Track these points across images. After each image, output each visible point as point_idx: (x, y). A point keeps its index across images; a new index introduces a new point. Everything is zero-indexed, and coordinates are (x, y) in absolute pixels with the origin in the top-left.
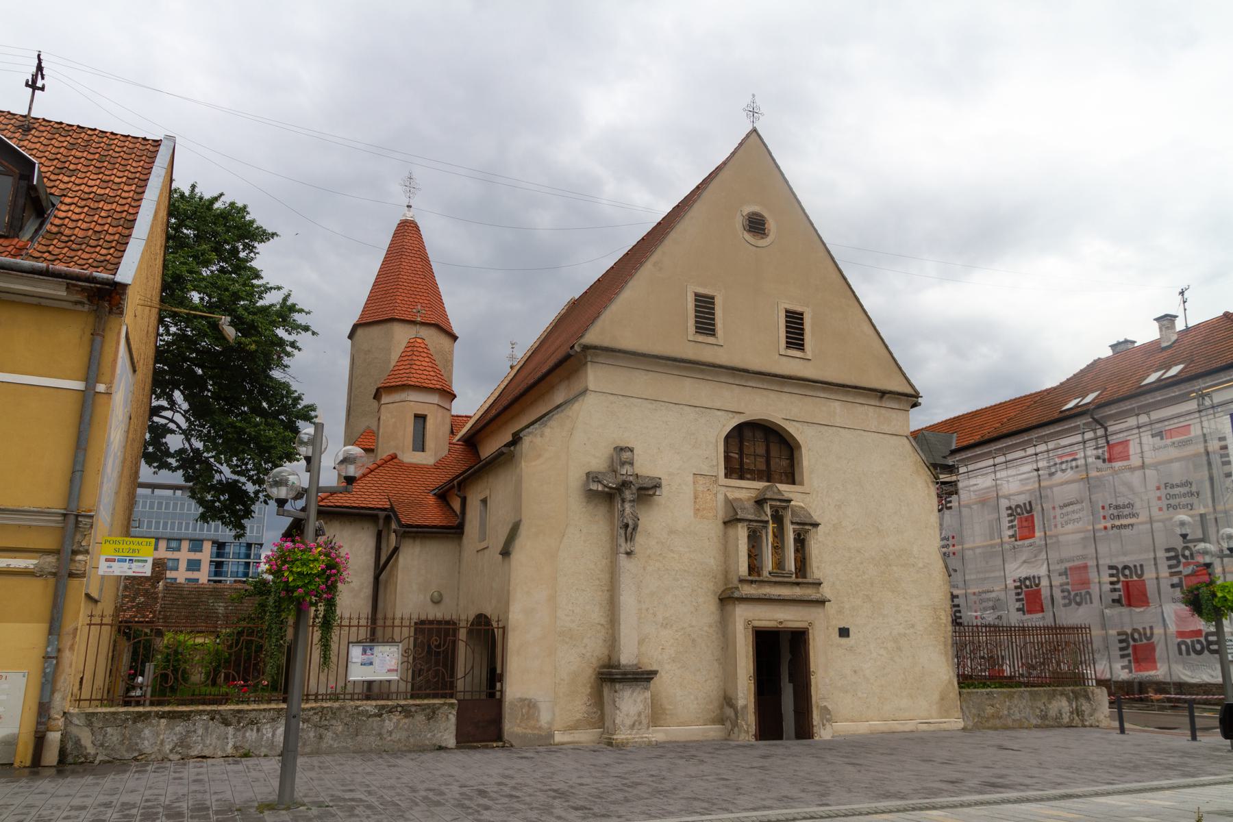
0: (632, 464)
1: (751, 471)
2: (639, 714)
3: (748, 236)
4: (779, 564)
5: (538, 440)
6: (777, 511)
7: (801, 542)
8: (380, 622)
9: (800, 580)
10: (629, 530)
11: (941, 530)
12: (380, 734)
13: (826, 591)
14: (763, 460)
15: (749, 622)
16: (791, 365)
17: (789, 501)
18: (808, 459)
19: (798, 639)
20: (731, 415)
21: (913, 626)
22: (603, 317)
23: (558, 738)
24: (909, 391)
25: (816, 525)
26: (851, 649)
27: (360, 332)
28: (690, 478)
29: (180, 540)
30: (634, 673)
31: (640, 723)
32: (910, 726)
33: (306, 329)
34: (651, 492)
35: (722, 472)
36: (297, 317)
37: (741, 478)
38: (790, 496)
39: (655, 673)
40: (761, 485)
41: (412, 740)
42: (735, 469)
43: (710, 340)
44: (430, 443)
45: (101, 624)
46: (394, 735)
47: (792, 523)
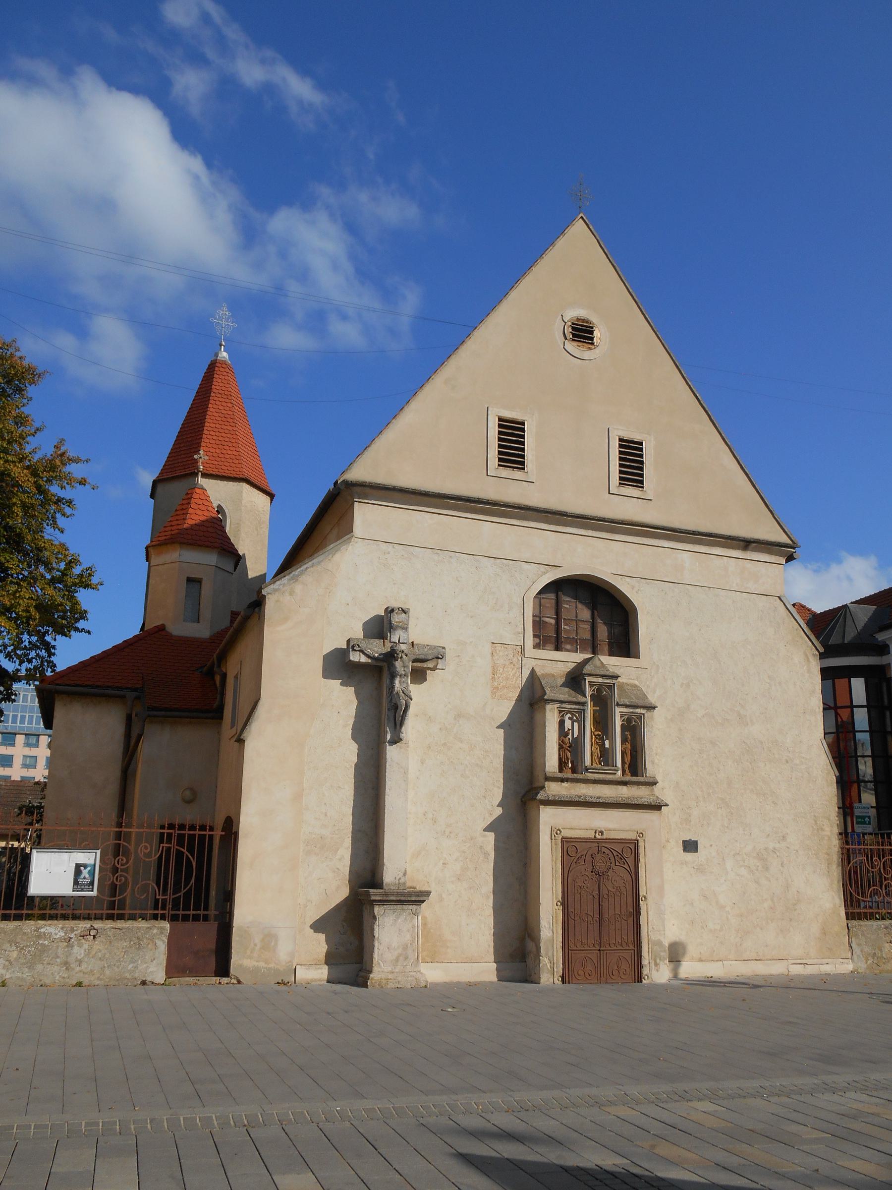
0: (405, 629)
1: (572, 641)
2: (405, 948)
4: (605, 756)
5: (286, 599)
9: (628, 778)
12: (66, 963)
13: (663, 792)
14: (588, 627)
16: (626, 505)
17: (616, 677)
18: (646, 628)
19: (626, 854)
20: (542, 568)
21: (784, 838)
22: (374, 447)
25: (651, 708)
26: (700, 869)
27: (160, 489)
28: (488, 648)
29: (39, 735)
30: (398, 894)
31: (406, 958)
32: (776, 969)
33: (83, 482)
34: (430, 665)
35: (530, 641)
36: (74, 469)
37: (557, 649)
38: (617, 671)
39: (428, 894)
41: (107, 972)
42: (549, 635)
43: (518, 474)
44: (206, 613)
46: (84, 965)
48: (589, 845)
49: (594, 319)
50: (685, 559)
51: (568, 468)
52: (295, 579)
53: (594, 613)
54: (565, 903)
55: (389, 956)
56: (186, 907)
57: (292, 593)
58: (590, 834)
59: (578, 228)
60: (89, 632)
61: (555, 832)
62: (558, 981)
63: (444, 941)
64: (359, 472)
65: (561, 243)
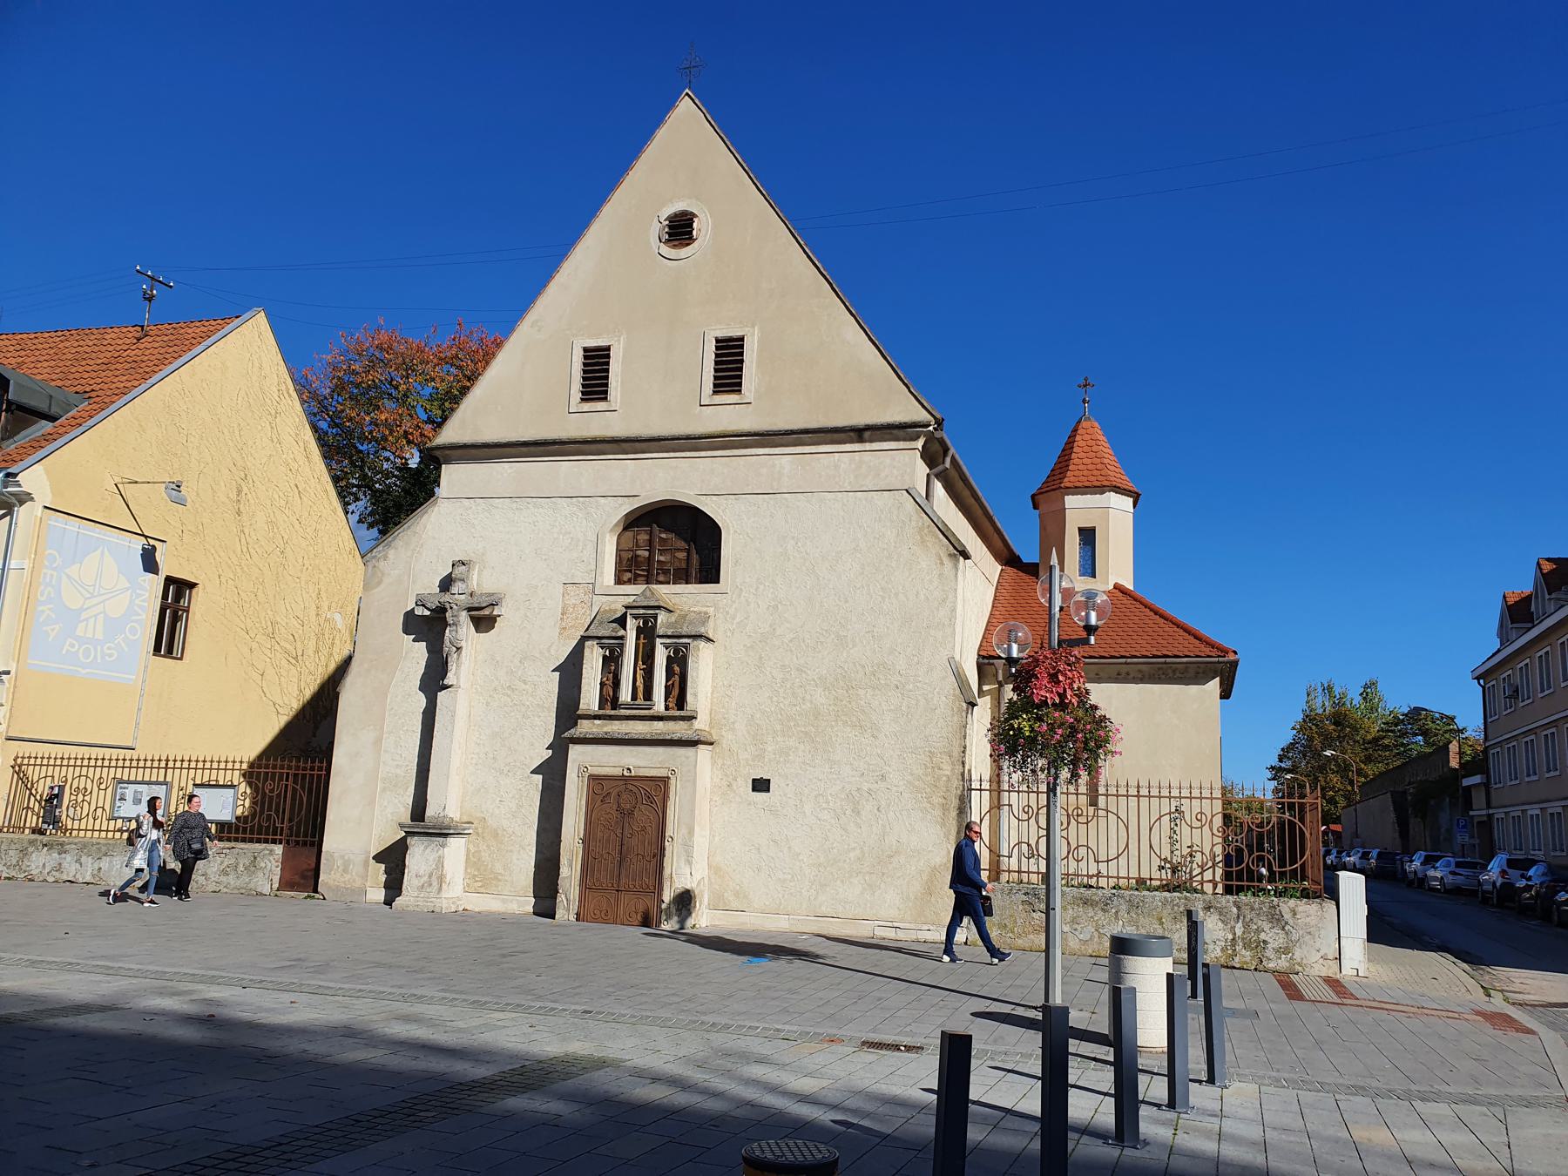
8: (1102, 790)
16: (727, 415)
19: (655, 791)
28: (560, 588)
40: (638, 589)
42: (631, 568)
43: (600, 406)
48: (615, 783)
50: (783, 463)
51: (659, 387)
52: (389, 545)
53: (675, 541)
54: (586, 841)
55: (416, 882)
56: (252, 832)
57: (386, 557)
58: (617, 772)
59: (686, 110)
61: (583, 769)
62: (572, 917)
63: (479, 875)
64: (452, 433)
65: (662, 134)
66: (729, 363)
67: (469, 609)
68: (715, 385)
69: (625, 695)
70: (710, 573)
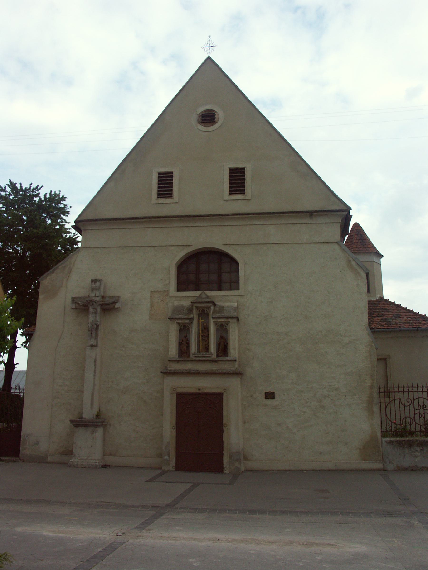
3: (200, 127)
6: (203, 311)
7: (223, 329)
10: (94, 330)
11: (151, 310)
15: (174, 389)
16: (237, 204)
23: (49, 459)
24: (345, 208)
28: (148, 295)
40: (197, 294)
43: (168, 200)
45: (404, 392)
47: (213, 318)
49: (215, 108)
50: (273, 231)
60: (210, 37)
66: (237, 181)
67: (102, 305)
68: (230, 191)
69: (193, 349)
70: (234, 284)
